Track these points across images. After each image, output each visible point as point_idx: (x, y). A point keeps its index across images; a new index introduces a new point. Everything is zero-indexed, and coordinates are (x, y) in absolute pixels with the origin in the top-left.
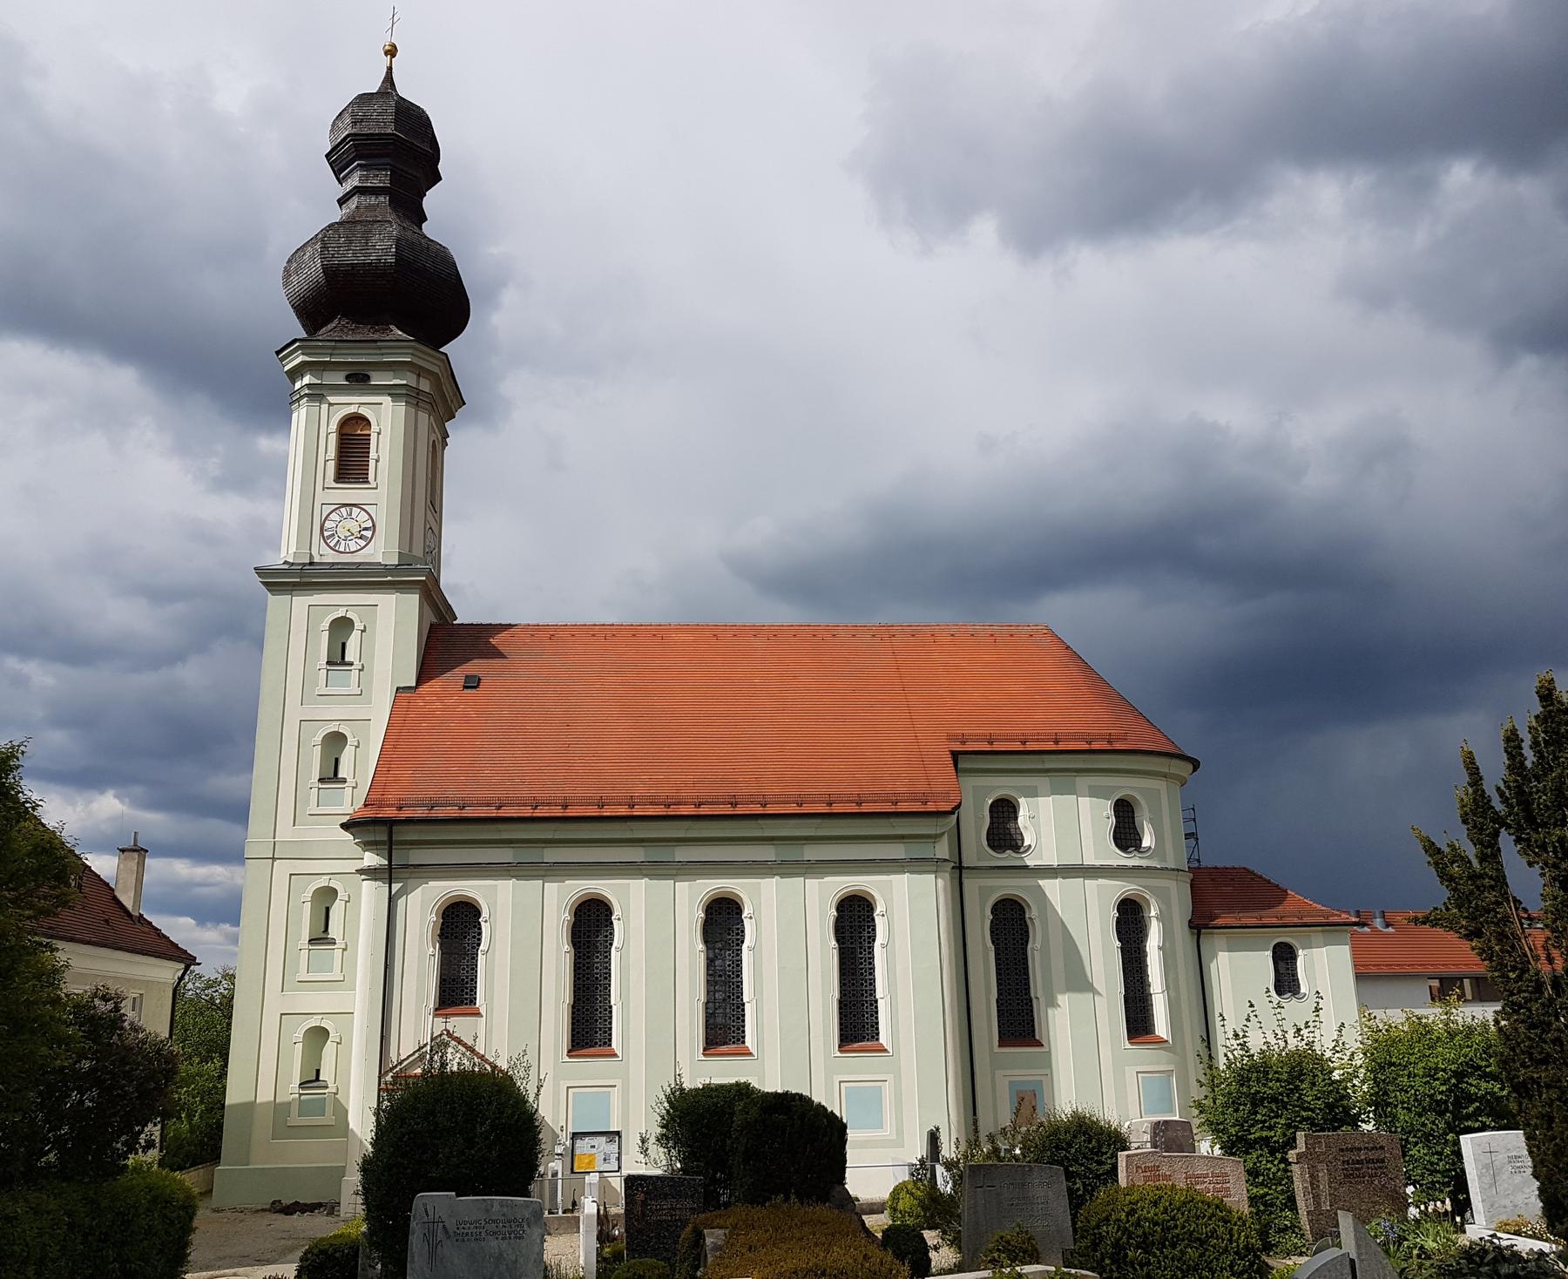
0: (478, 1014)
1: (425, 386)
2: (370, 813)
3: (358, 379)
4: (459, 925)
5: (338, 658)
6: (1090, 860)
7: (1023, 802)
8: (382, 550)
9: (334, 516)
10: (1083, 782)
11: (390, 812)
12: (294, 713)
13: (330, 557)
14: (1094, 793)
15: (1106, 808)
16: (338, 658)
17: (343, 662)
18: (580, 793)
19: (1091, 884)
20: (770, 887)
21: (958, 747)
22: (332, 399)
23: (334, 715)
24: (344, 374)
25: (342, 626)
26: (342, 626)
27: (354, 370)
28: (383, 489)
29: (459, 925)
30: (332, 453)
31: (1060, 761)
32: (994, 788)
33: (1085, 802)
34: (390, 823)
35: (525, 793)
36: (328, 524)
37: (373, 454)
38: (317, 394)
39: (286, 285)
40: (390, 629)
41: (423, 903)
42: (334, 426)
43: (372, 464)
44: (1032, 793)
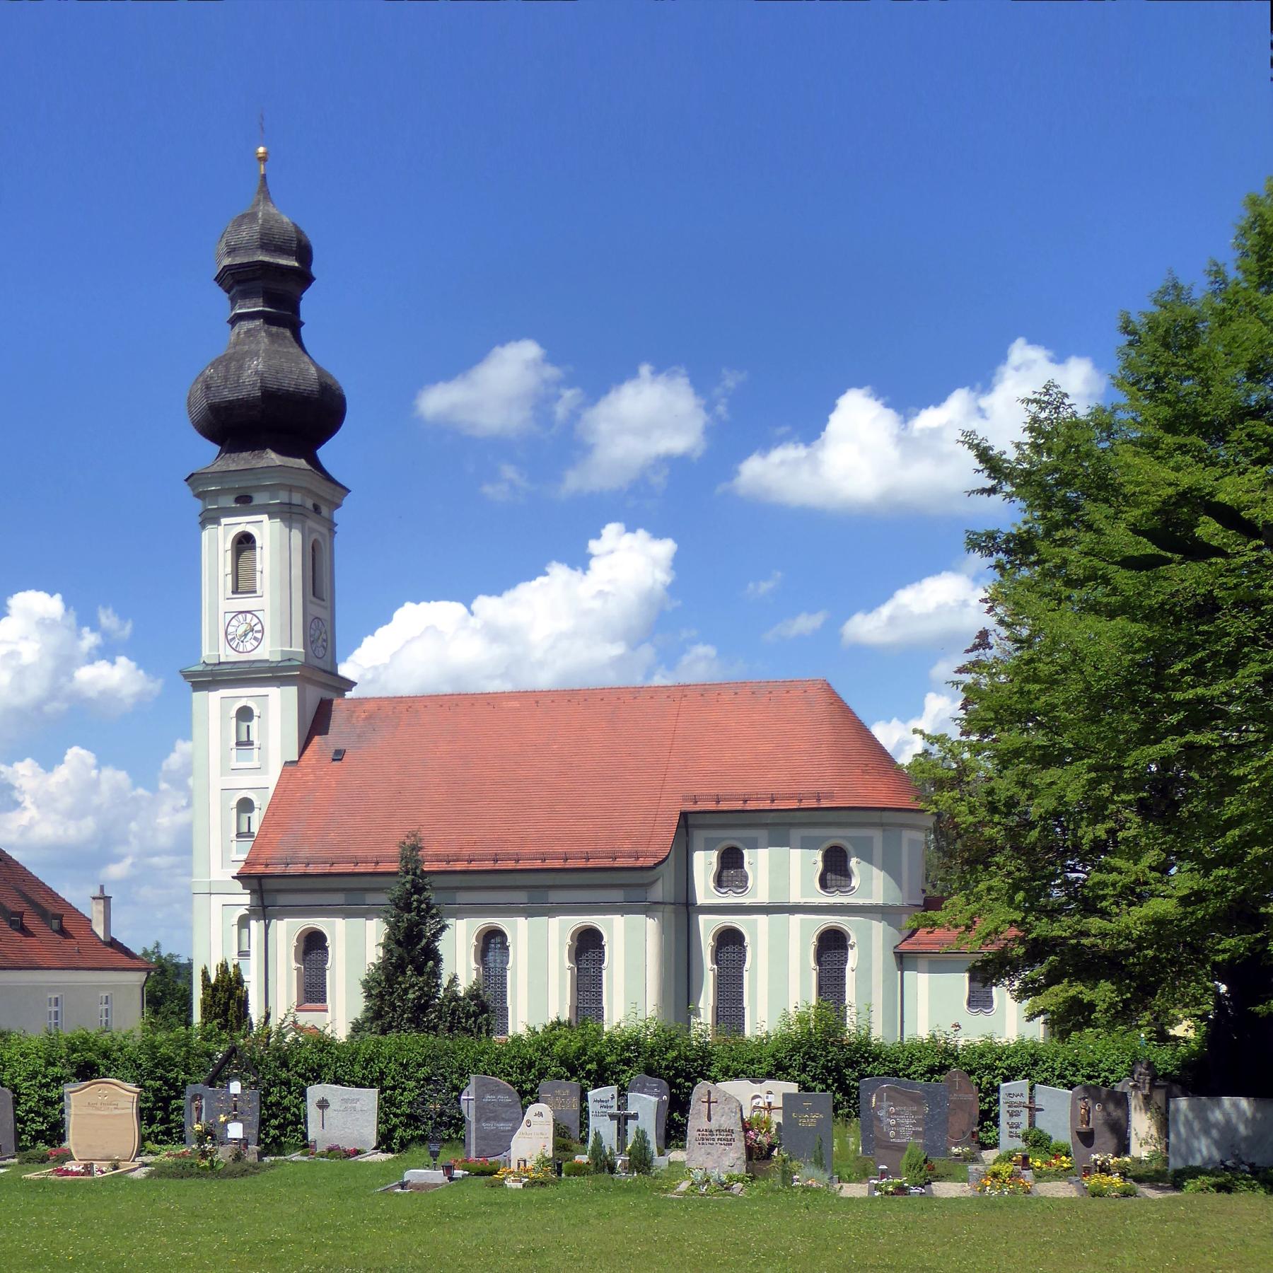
0: (326, 1011)
1: (297, 498)
2: (248, 871)
3: (244, 502)
4: (313, 944)
5: (244, 743)
6: (762, 919)
7: (745, 852)
8: (267, 650)
9: (234, 622)
10: (796, 834)
11: (260, 869)
12: (217, 781)
13: (233, 657)
14: (806, 844)
15: (818, 855)
16: (244, 743)
17: (249, 743)
18: (575, 849)
19: (797, 919)
20: (521, 922)
21: (689, 807)
22: (224, 521)
23: (245, 784)
24: (232, 498)
25: (245, 714)
26: (245, 714)
27: (242, 493)
28: (267, 596)
29: (313, 944)
30: (229, 569)
31: (780, 825)
32: (724, 839)
33: (796, 855)
34: (260, 878)
35: (559, 849)
36: (231, 629)
37: (259, 567)
38: (210, 518)
39: (190, 412)
40: (278, 709)
41: (287, 931)
42: (229, 545)
43: (258, 574)
44: (754, 845)
